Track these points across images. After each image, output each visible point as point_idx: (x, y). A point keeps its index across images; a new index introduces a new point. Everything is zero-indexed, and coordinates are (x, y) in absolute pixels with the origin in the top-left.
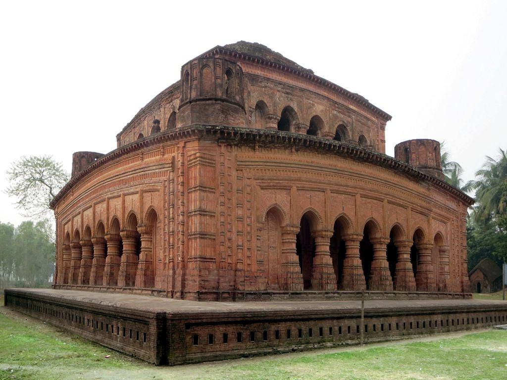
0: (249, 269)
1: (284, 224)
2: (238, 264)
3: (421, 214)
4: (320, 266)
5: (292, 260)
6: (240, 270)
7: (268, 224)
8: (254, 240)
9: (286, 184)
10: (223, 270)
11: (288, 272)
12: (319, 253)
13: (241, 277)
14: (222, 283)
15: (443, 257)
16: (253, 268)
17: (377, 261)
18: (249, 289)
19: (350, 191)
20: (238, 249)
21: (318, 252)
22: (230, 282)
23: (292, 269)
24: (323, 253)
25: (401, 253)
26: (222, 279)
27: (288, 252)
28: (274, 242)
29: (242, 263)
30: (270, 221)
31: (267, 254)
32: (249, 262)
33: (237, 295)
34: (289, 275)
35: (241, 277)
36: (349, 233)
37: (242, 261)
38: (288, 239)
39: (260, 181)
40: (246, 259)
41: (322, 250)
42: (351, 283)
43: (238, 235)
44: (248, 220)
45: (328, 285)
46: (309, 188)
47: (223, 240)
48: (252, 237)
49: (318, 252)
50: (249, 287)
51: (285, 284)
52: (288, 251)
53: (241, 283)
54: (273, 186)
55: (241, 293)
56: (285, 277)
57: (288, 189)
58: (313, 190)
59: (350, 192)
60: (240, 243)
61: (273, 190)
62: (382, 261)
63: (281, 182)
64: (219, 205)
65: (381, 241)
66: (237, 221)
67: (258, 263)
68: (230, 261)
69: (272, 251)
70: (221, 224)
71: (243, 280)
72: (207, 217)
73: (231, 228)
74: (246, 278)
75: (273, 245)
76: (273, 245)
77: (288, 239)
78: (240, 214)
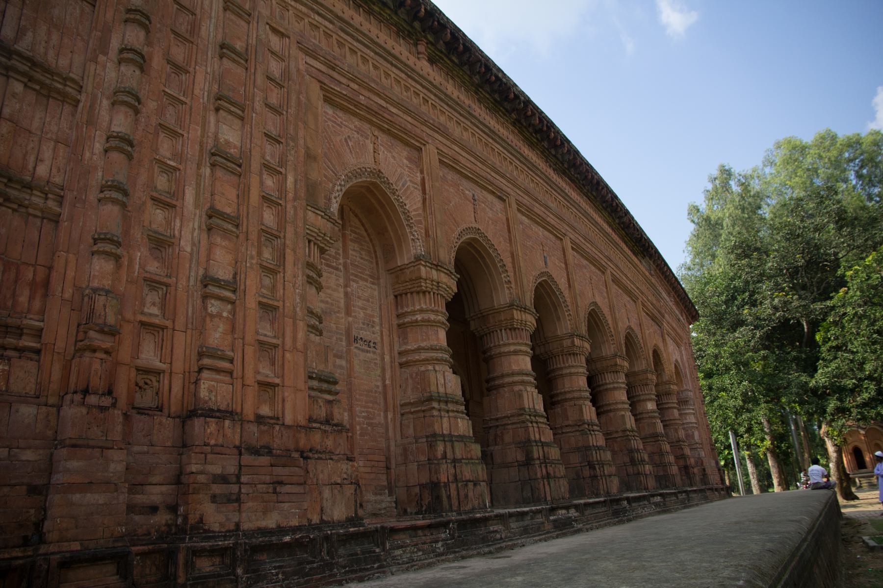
0: (265, 410)
1: (402, 259)
2: (205, 374)
3: (653, 320)
4: (515, 419)
5: (441, 390)
6: (209, 413)
7: (345, 251)
8: (294, 272)
9: (409, 126)
10: (92, 399)
11: (434, 435)
12: (508, 380)
13: (218, 450)
14: (72, 488)
15: (686, 414)
16: (288, 406)
17: (611, 414)
18: (271, 522)
19: (553, 222)
20: (205, 297)
21: (503, 376)
22: (135, 487)
23: (444, 426)
24: (516, 378)
25: (606, 389)
26: (74, 464)
27: (427, 361)
28: (370, 324)
29: (231, 373)
30: (351, 245)
31: (344, 363)
32: (267, 372)
33: (189, 565)
34: (440, 448)
35: (218, 450)
36: (559, 333)
37: (226, 365)
38: (422, 311)
39: (323, 68)
40: (250, 351)
41: (515, 368)
42: (587, 472)
43: (209, 229)
44: (269, 182)
45: (601, 451)
46: (472, 171)
47: (114, 227)
48: (282, 257)
49: (503, 376)
50: (266, 512)
51: (422, 486)
52: (423, 355)
53: (217, 489)
54: (368, 109)
55: (212, 552)
56: (423, 458)
57: (416, 148)
58: (476, 183)
59: (553, 227)
60: (223, 273)
61: (366, 127)
62: (623, 413)
63: (394, 110)
64: (113, 52)
65: (616, 365)
66: (213, 165)
67: (315, 383)
68: (149, 356)
69: (363, 356)
70: (114, 143)
71: (232, 469)
72: (18, 87)
73: (178, 194)
74: (247, 459)
75: (365, 334)
76: (363, 334)
77: (422, 311)
78: (227, 142)
